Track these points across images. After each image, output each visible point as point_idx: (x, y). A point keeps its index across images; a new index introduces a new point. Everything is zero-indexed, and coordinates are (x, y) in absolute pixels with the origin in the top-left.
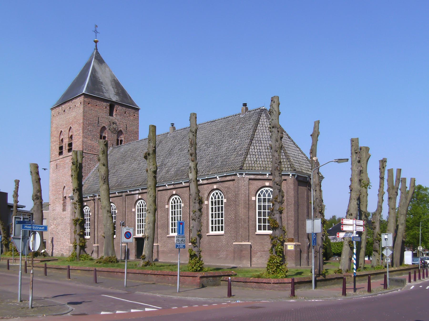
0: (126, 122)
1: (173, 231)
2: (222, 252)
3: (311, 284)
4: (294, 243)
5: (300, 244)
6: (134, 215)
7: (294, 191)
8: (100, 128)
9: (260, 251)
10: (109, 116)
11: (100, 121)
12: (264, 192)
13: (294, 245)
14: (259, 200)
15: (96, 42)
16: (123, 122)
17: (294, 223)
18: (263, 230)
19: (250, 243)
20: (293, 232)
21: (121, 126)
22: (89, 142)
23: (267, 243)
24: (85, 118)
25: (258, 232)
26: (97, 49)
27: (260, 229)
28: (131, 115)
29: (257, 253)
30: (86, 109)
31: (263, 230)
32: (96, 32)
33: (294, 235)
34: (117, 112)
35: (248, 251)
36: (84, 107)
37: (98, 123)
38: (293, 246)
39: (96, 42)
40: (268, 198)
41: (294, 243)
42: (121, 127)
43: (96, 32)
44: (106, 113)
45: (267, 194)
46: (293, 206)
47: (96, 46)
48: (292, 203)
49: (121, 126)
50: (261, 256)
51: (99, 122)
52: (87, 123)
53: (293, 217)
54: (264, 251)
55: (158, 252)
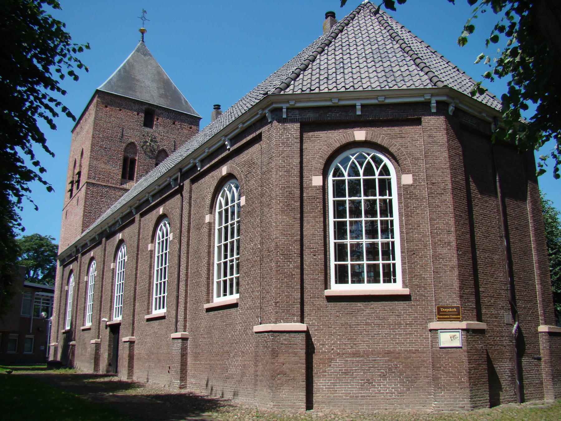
0: (175, 137)
1: (161, 303)
2: (234, 357)
3: (520, 203)
4: (463, 325)
5: (482, 325)
6: (113, 276)
7: (449, 150)
8: (124, 145)
9: (343, 354)
10: (143, 127)
11: (126, 134)
12: (353, 162)
13: (462, 330)
14: (339, 189)
15: (143, 32)
16: (168, 137)
17: (458, 255)
18: (352, 283)
19: (303, 327)
20: (456, 285)
21: (166, 143)
22: (103, 166)
23: (367, 324)
24: (98, 128)
25: (336, 289)
26: (143, 41)
27: (342, 278)
28: (184, 127)
29: (330, 360)
30: (100, 114)
31: (352, 283)
32: (143, 19)
33: (461, 297)
34: (159, 121)
35: (296, 354)
36: (97, 110)
37: (122, 137)
38: (458, 335)
39: (143, 32)
40: (364, 180)
41: (463, 325)
42: (165, 145)
43: (143, 18)
44: (137, 121)
45: (361, 169)
46: (448, 197)
47: (143, 37)
48: (444, 189)
49: (166, 143)
50: (346, 373)
51: (123, 135)
52: (101, 136)
53: (453, 234)
54: (356, 354)
55: (131, 357)
